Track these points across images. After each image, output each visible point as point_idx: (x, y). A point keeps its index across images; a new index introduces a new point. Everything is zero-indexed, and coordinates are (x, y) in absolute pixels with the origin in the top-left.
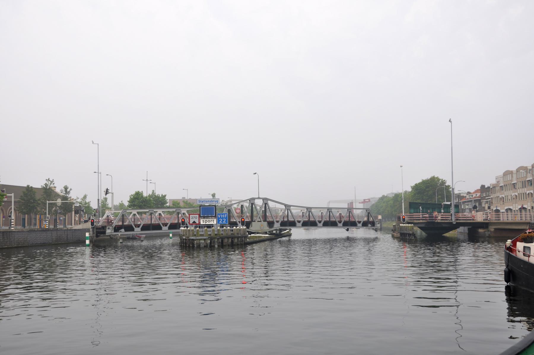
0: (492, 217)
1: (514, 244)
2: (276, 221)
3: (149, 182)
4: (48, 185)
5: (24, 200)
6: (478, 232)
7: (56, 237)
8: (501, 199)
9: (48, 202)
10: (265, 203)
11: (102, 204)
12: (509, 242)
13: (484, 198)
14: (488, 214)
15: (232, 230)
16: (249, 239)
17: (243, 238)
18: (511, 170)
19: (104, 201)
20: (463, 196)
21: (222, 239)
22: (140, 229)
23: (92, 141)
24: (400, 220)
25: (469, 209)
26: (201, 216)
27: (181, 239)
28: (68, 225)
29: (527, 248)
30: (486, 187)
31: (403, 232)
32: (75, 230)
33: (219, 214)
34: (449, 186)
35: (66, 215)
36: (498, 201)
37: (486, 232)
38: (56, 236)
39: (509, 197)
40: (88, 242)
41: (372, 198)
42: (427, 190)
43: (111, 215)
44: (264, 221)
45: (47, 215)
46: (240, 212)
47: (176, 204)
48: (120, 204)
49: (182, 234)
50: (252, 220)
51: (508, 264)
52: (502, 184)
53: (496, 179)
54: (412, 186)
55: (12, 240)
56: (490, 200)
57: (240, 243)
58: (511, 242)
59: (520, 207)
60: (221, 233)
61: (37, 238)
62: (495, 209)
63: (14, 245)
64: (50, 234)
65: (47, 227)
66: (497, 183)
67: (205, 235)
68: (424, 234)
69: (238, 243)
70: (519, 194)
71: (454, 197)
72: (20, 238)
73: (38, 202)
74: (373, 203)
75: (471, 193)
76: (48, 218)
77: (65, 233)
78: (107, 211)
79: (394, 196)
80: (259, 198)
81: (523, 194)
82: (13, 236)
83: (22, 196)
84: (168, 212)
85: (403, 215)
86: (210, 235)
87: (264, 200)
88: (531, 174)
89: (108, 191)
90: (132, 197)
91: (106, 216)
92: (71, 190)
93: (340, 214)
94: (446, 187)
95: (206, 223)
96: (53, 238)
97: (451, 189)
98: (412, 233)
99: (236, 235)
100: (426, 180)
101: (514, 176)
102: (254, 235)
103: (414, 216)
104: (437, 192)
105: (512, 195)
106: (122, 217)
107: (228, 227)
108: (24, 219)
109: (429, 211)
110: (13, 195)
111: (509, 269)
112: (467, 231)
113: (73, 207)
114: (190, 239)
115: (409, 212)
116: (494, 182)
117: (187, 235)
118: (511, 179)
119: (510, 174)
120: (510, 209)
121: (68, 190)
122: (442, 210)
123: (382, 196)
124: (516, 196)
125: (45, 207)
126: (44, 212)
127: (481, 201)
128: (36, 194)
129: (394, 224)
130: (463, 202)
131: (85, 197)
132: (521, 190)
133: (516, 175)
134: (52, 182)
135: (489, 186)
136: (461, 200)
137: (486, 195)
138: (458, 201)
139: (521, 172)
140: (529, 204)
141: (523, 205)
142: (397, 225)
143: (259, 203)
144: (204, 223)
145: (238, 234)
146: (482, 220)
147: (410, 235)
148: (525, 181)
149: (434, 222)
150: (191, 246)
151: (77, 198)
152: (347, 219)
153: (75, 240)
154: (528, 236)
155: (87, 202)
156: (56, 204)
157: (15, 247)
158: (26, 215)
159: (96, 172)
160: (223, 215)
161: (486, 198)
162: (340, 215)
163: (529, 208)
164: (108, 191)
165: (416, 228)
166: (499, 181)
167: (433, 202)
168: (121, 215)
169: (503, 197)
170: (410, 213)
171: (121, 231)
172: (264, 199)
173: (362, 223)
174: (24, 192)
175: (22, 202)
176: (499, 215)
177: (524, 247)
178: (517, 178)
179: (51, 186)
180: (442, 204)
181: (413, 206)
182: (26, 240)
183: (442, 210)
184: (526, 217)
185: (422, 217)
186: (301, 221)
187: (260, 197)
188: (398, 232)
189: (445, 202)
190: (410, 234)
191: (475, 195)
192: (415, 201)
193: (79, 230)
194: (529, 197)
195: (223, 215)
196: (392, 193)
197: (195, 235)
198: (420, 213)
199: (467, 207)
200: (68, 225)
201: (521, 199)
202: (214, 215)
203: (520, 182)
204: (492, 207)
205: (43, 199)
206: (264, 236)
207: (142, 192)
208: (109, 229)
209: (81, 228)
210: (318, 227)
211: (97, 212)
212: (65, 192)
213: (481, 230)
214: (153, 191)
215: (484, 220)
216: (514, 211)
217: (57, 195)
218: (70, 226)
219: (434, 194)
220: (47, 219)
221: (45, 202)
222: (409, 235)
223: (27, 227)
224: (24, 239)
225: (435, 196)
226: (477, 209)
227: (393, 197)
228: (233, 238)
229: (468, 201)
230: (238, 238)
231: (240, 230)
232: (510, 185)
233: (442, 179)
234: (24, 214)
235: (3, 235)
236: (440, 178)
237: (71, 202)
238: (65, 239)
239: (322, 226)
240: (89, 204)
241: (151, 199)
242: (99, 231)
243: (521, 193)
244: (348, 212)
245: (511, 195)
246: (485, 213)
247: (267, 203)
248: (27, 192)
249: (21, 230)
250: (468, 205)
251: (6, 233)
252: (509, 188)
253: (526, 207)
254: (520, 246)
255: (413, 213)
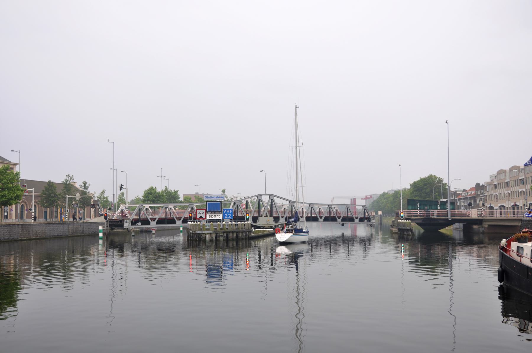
0: (486, 214)
1: (509, 245)
2: (281, 216)
3: (163, 178)
4: (68, 180)
5: (45, 194)
6: (473, 228)
7: (73, 230)
8: (495, 196)
9: (67, 196)
10: (271, 200)
11: (119, 198)
12: (504, 242)
13: (478, 195)
14: (483, 211)
15: (237, 225)
16: (254, 233)
17: (248, 232)
18: (504, 169)
19: (121, 196)
20: (459, 193)
21: (228, 233)
22: (181, 222)
23: (108, 140)
24: (398, 216)
25: (465, 205)
26: (208, 211)
27: (188, 233)
28: (87, 218)
29: (520, 248)
30: (481, 185)
31: (401, 228)
32: (91, 223)
33: (225, 210)
34: (446, 184)
35: (85, 208)
36: (492, 199)
37: (480, 229)
38: (72, 228)
39: (503, 195)
40: (101, 235)
41: (374, 195)
42: (425, 187)
43: (125, 209)
44: (270, 216)
45: (67, 209)
46: (245, 208)
47: (188, 199)
48: (136, 198)
49: (189, 228)
50: (259, 215)
51: (502, 264)
52: (495, 183)
53: (490, 177)
54: (411, 183)
55: (31, 232)
56: (484, 197)
57: (244, 237)
58: (506, 242)
59: (513, 204)
60: (226, 227)
61: (55, 230)
62: (489, 206)
63: (32, 237)
64: (67, 227)
65: (67, 220)
66: (491, 181)
67: (210, 230)
68: (422, 231)
69: (243, 237)
70: (512, 192)
71: (450, 194)
72: (38, 230)
73: (59, 196)
74: (375, 199)
75: (466, 191)
76: (68, 212)
77: (81, 225)
78: (122, 205)
79: (394, 192)
80: (266, 194)
81: (516, 192)
82: (32, 228)
83: (43, 191)
84: (180, 207)
85: (402, 211)
86: (216, 229)
87: (270, 196)
88: (524, 174)
89: (122, 187)
90: (146, 192)
91: (120, 210)
92: (89, 185)
93: (336, 210)
94: (443, 185)
95: (213, 218)
96: (69, 230)
97: (447, 187)
98: (409, 229)
99: (241, 229)
100: (424, 178)
101: (508, 175)
102: (258, 229)
103: (412, 213)
104: (434, 190)
105: (506, 193)
106: (138, 211)
107: (233, 222)
108: (46, 212)
109: (426, 208)
110: (33, 190)
111: (502, 269)
112: (463, 227)
113: (92, 201)
114: (197, 233)
115: (407, 209)
116: (488, 180)
117: (193, 229)
118: (504, 178)
119: (504, 173)
120: (503, 206)
121: (87, 185)
122: (439, 207)
123: (382, 193)
124: (509, 193)
125: (65, 201)
126: (64, 205)
127: (476, 198)
128: (56, 189)
129: (393, 220)
130: (458, 199)
131: (103, 192)
132: (514, 188)
133: (509, 174)
134: (71, 178)
135: (484, 184)
136: (457, 197)
137: (481, 193)
138: (455, 198)
139: (514, 171)
140: (521, 201)
141: (515, 203)
142: (396, 221)
143: (266, 199)
144: (211, 218)
145: (242, 228)
146: (477, 217)
147: (407, 230)
148: (518, 180)
149: (431, 219)
150: (197, 239)
151: (95, 192)
152: (326, 215)
153: (91, 233)
154: (522, 236)
155: (105, 196)
156: (75, 198)
157: (34, 238)
158: (48, 209)
159: (112, 169)
160: (228, 211)
161: (481, 195)
162: (336, 211)
163: (521, 205)
164: (122, 187)
165: (413, 224)
166: (493, 180)
167: (430, 199)
168: (138, 209)
169: (496, 195)
170: (408, 210)
171: (138, 225)
172: (270, 195)
173: (359, 218)
174: (45, 187)
175: (44, 196)
176: (493, 212)
177: (518, 247)
178: (510, 177)
179: (71, 181)
180: (439, 201)
181: (411, 203)
182: (44, 233)
183: (439, 207)
184: (525, 215)
185: (420, 214)
186: (322, 216)
187: (267, 193)
188: (397, 228)
189: (441, 199)
190: (408, 230)
191: (471, 193)
192: (413, 198)
193: (94, 223)
194: (521, 195)
195: (228, 211)
196: (393, 190)
197: (201, 230)
198: (418, 209)
199: (462, 204)
200: (87, 218)
201: (516, 197)
202: (220, 211)
203: (513, 180)
204: (486, 204)
205: (63, 193)
206: (269, 231)
207: (156, 187)
208: (126, 222)
209: (97, 222)
210: (319, 222)
211: (112, 206)
212: (83, 187)
213: (475, 227)
214: (166, 187)
215: (478, 216)
216: (507, 208)
217: (77, 190)
218: (88, 219)
219: (432, 191)
220: (66, 212)
221: (65, 197)
222: (407, 231)
223: (48, 220)
224: (42, 231)
225: (432, 193)
226: (472, 206)
227: (393, 194)
228: (237, 233)
229: (464, 199)
230: (242, 232)
231: (245, 225)
232: (503, 184)
233: (439, 178)
234: (46, 207)
235: (22, 228)
236: (438, 176)
237: (89, 197)
238: (82, 231)
239: (323, 221)
240: (107, 199)
241: (165, 194)
242: (116, 224)
243: (514, 191)
244: (347, 208)
245: (505, 193)
246: (480, 210)
247: (273, 200)
248: (48, 187)
249: (39, 223)
250: (463, 202)
251: (25, 225)
252: (502, 186)
253: (519, 205)
254: (514, 245)
255: (411, 210)
